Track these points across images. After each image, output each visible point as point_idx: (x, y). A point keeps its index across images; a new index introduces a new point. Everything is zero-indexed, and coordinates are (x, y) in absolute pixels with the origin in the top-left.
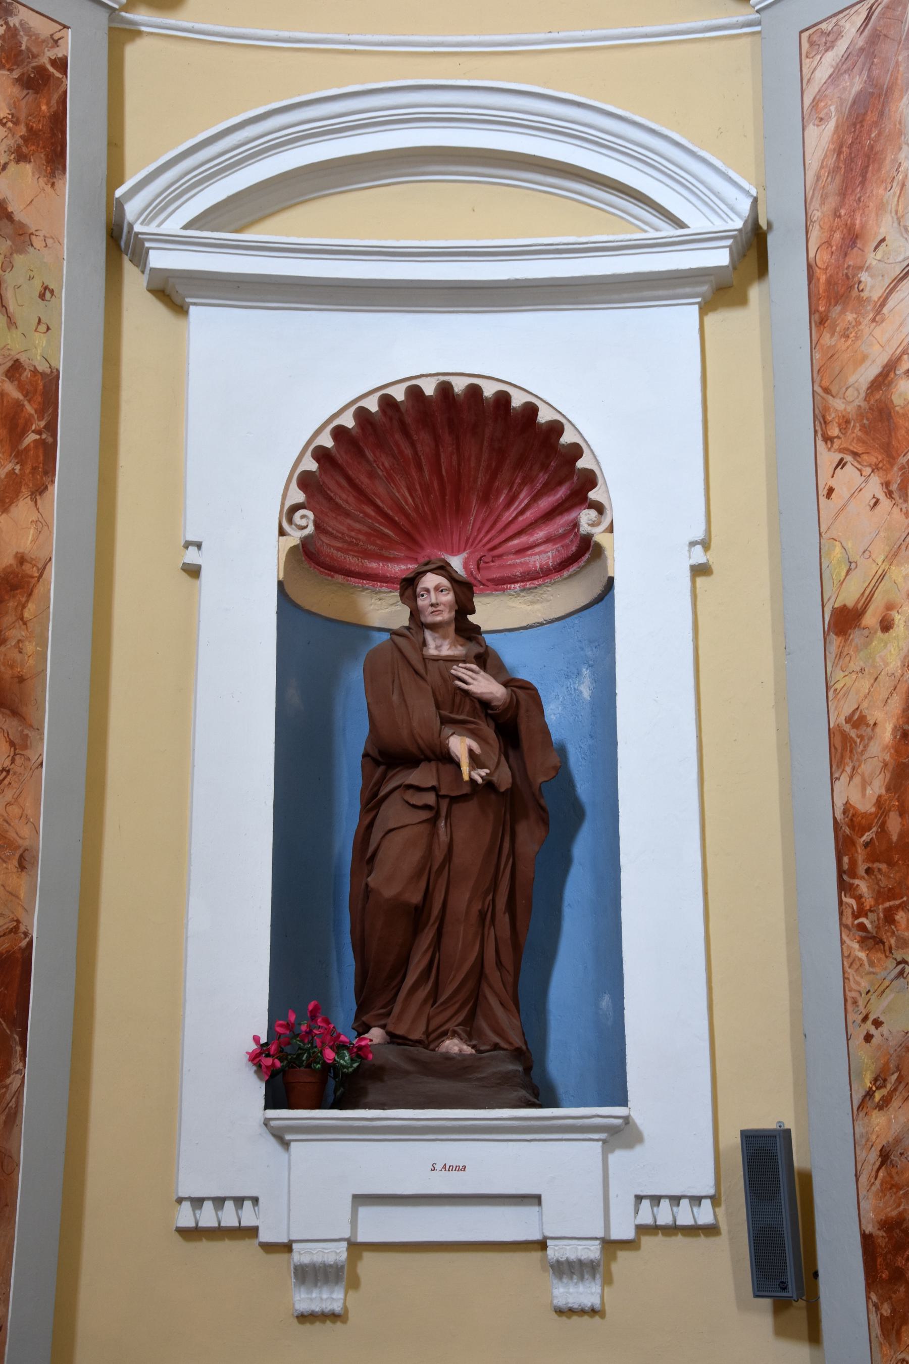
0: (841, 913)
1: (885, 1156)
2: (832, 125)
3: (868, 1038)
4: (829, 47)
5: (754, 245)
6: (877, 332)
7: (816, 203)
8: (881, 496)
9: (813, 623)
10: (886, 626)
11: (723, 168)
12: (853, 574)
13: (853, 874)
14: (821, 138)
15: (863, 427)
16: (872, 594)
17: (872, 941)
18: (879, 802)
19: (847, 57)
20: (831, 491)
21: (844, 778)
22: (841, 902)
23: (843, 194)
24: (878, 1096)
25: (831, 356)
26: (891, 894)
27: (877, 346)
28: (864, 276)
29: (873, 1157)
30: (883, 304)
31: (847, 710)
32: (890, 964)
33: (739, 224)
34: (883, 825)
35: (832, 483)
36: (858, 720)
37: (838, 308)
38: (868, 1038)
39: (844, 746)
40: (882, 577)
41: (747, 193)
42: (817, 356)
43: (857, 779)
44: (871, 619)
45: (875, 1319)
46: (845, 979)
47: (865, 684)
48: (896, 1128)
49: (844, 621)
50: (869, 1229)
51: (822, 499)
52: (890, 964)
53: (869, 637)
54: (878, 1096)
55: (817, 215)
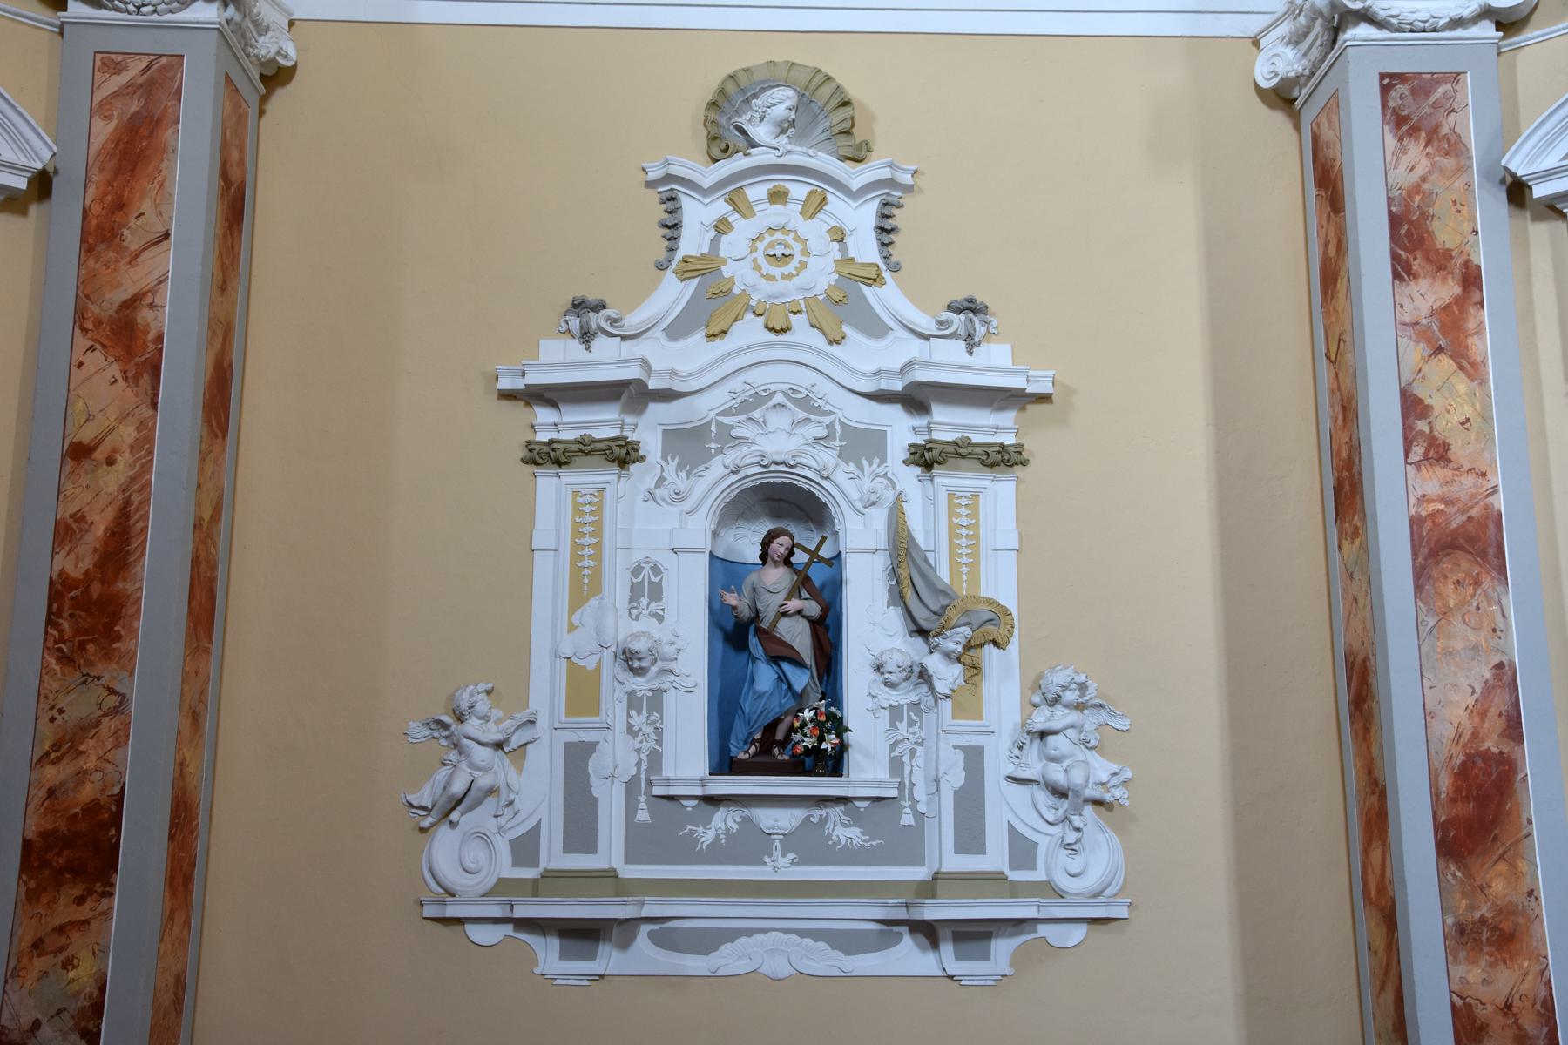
0: (45, 640)
1: (51, 793)
2: (113, 124)
3: (52, 720)
4: (118, 72)
5: (42, 183)
6: (132, 271)
7: (96, 169)
8: (119, 376)
9: (56, 449)
10: (110, 462)
11: (33, 122)
12: (89, 424)
13: (59, 614)
14: (103, 130)
15: (112, 329)
16: (102, 440)
17: (66, 660)
18: (87, 573)
19: (128, 86)
20: (81, 365)
21: (63, 553)
22: (46, 632)
23: (117, 172)
24: (53, 756)
25: (94, 275)
26: (86, 632)
27: (131, 281)
28: (126, 232)
29: (42, 793)
30: (138, 255)
31: (72, 510)
32: (78, 675)
33: (40, 166)
34: (87, 588)
35: (84, 359)
36: (79, 518)
37: (103, 246)
38: (52, 720)
39: (66, 532)
40: (113, 429)
41: (50, 148)
42: (83, 272)
43: (72, 556)
44: (100, 454)
45: (22, 890)
46: (41, 681)
47: (89, 496)
48: (62, 776)
49: (79, 452)
50: (30, 836)
51: (74, 368)
52: (78, 675)
53: (97, 465)
54: (53, 756)
55: (95, 178)
